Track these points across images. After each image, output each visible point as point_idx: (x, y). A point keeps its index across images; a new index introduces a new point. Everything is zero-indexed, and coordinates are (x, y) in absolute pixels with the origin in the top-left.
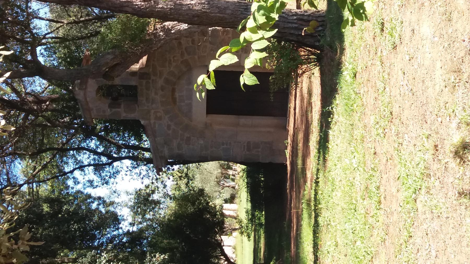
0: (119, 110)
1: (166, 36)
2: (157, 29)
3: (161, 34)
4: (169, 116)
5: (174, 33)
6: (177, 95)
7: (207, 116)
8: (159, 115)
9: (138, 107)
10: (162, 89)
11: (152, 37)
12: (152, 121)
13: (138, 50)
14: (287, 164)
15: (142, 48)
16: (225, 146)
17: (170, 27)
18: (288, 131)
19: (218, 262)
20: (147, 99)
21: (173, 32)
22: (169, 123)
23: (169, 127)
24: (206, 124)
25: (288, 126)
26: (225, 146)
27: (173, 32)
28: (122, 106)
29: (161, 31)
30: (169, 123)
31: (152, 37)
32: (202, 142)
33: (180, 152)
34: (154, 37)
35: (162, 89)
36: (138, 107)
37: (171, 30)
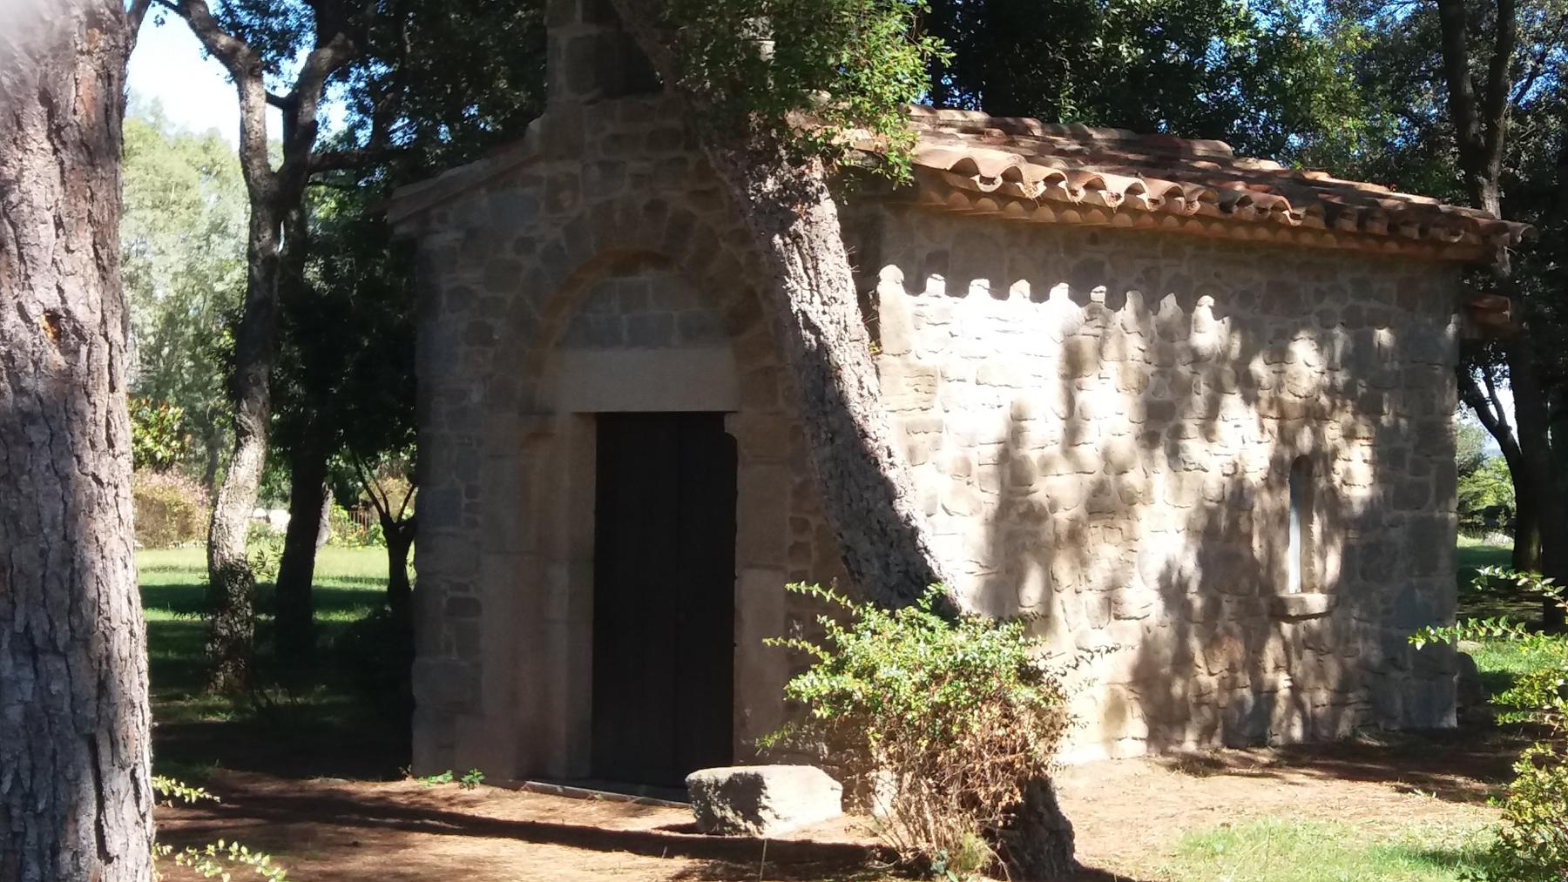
0: (578, 16)
1: (759, 210)
2: (796, 162)
3: (770, 185)
4: (563, 244)
5: (772, 246)
6: (647, 276)
7: (581, 415)
8: (565, 197)
9: (590, 102)
10: (656, 207)
11: (756, 144)
12: (542, 170)
13: (700, 79)
14: (403, 778)
15: (707, 95)
16: (465, 501)
17: (799, 226)
18: (516, 789)
19: (1360, 326)
20: (616, 138)
21: (777, 239)
22: (540, 248)
23: (525, 245)
24: (548, 413)
25: (534, 789)
26: (465, 501)
27: (777, 239)
28: (593, 30)
29: (786, 185)
30: (540, 248)
31: (756, 144)
32: (476, 397)
33: (444, 300)
34: (755, 151)
35: (656, 207)
36: (590, 102)
37: (784, 232)
